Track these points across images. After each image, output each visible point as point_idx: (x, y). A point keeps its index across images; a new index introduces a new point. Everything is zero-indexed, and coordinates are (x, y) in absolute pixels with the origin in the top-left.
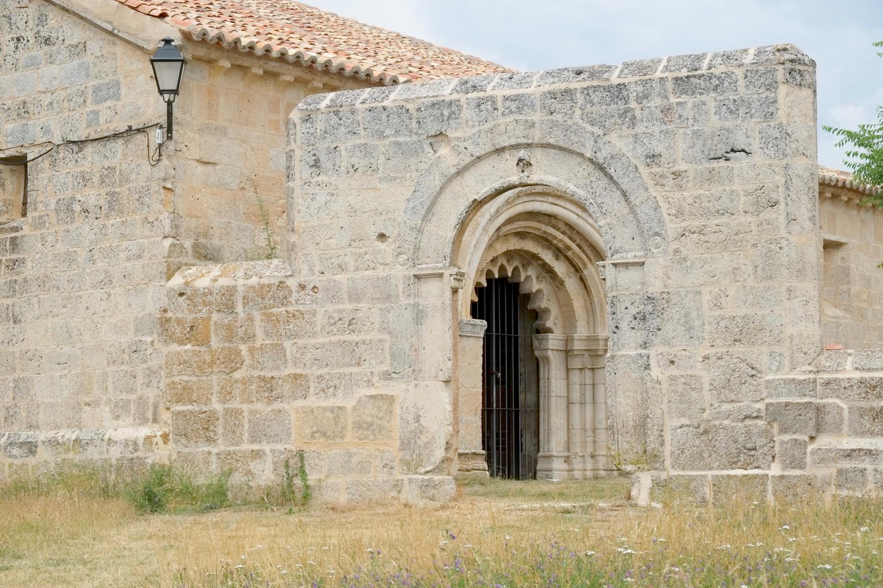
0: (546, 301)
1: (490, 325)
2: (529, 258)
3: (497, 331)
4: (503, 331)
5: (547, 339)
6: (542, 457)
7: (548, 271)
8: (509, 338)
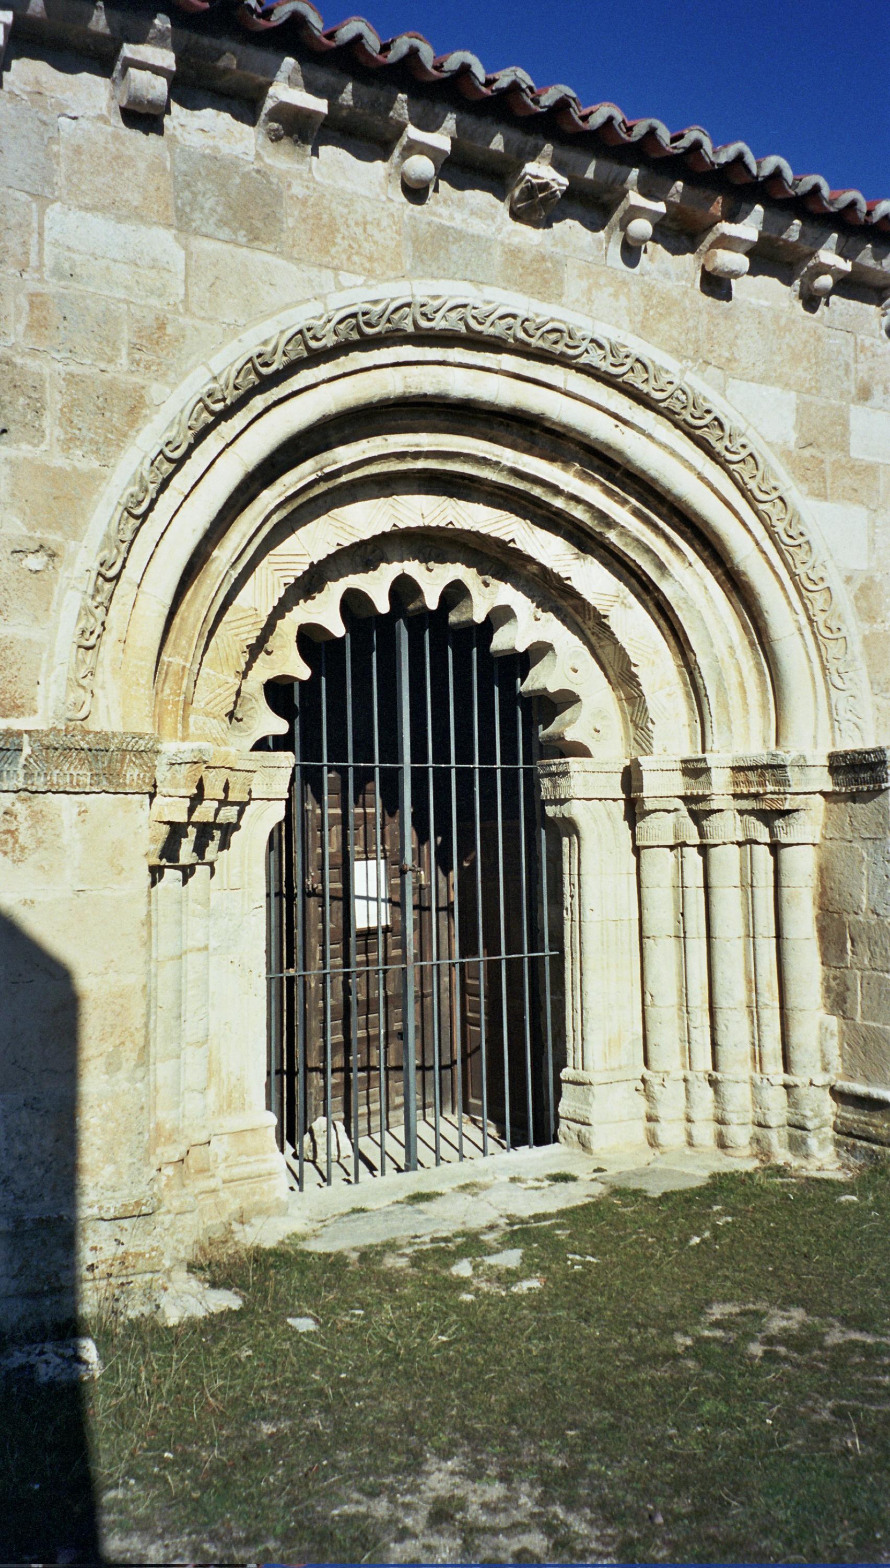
0: (566, 666)
4: (442, 754)
6: (569, 1082)
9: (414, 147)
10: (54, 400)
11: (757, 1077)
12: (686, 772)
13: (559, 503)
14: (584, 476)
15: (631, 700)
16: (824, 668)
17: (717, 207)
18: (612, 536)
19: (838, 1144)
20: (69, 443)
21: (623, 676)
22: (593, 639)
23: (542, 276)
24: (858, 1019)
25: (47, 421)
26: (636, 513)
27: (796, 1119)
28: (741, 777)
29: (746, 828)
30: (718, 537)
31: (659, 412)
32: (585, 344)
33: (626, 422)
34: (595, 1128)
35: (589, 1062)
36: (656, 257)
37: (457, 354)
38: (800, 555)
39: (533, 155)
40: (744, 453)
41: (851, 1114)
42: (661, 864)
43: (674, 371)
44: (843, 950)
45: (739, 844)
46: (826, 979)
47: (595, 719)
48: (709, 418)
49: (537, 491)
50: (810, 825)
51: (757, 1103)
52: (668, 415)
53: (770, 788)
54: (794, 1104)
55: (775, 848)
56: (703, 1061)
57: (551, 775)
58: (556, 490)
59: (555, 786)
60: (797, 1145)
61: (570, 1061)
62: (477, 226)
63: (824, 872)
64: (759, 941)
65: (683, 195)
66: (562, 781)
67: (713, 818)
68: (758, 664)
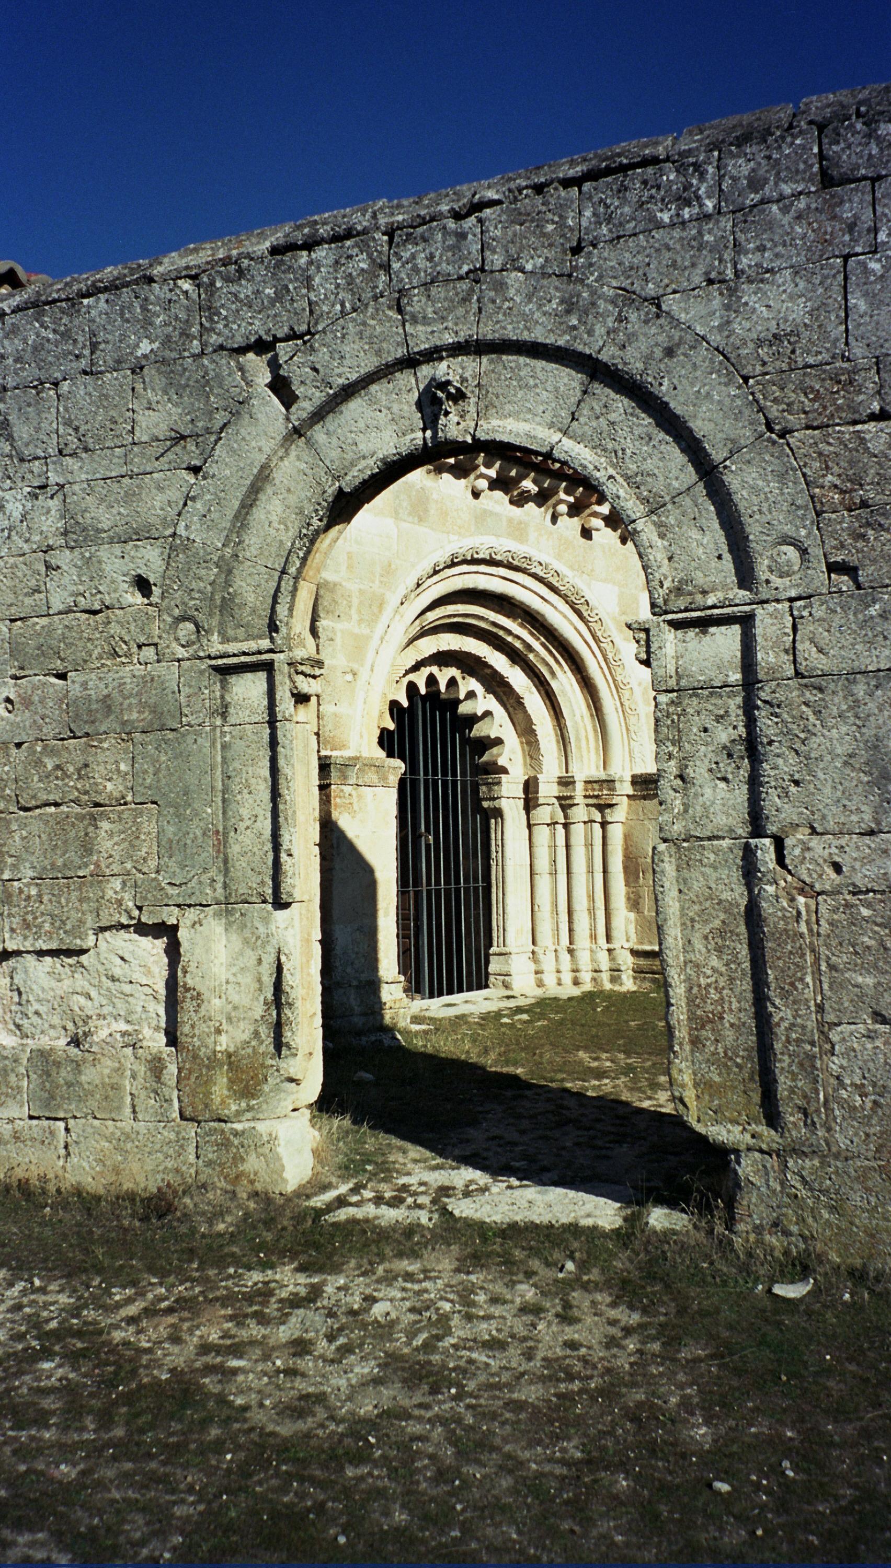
0: (499, 725)
1: (412, 768)
2: (471, 665)
3: (426, 773)
4: (435, 773)
5: (499, 783)
6: (495, 954)
7: (497, 685)
8: (445, 783)
9: (482, 476)
10: (355, 601)
11: (594, 946)
12: (560, 783)
13: (510, 639)
14: (522, 625)
15: (529, 743)
16: (628, 729)
17: (594, 499)
18: (531, 656)
19: (635, 978)
20: (360, 621)
21: (527, 731)
22: (511, 709)
23: (519, 531)
24: (646, 913)
25: (353, 612)
26: (543, 645)
27: (614, 967)
28: (590, 786)
29: (589, 813)
30: (582, 660)
31: (560, 596)
32: (536, 564)
33: (546, 600)
34: (514, 977)
35: (507, 942)
36: (564, 521)
37: (483, 568)
38: (619, 670)
39: (525, 477)
40: (597, 618)
41: (642, 962)
42: (542, 835)
43: (571, 578)
44: (638, 877)
45: (585, 823)
46: (628, 893)
47: (510, 755)
48: (583, 600)
49: (501, 633)
50: (620, 814)
51: (593, 960)
52: (565, 597)
53: (605, 792)
54: (612, 959)
55: (604, 824)
56: (565, 941)
57: (487, 784)
58: (509, 632)
59: (490, 790)
60: (613, 980)
61: (495, 943)
62: (498, 509)
63: (627, 837)
64: (595, 874)
65: (582, 494)
66: (496, 788)
67: (574, 808)
68: (594, 726)
